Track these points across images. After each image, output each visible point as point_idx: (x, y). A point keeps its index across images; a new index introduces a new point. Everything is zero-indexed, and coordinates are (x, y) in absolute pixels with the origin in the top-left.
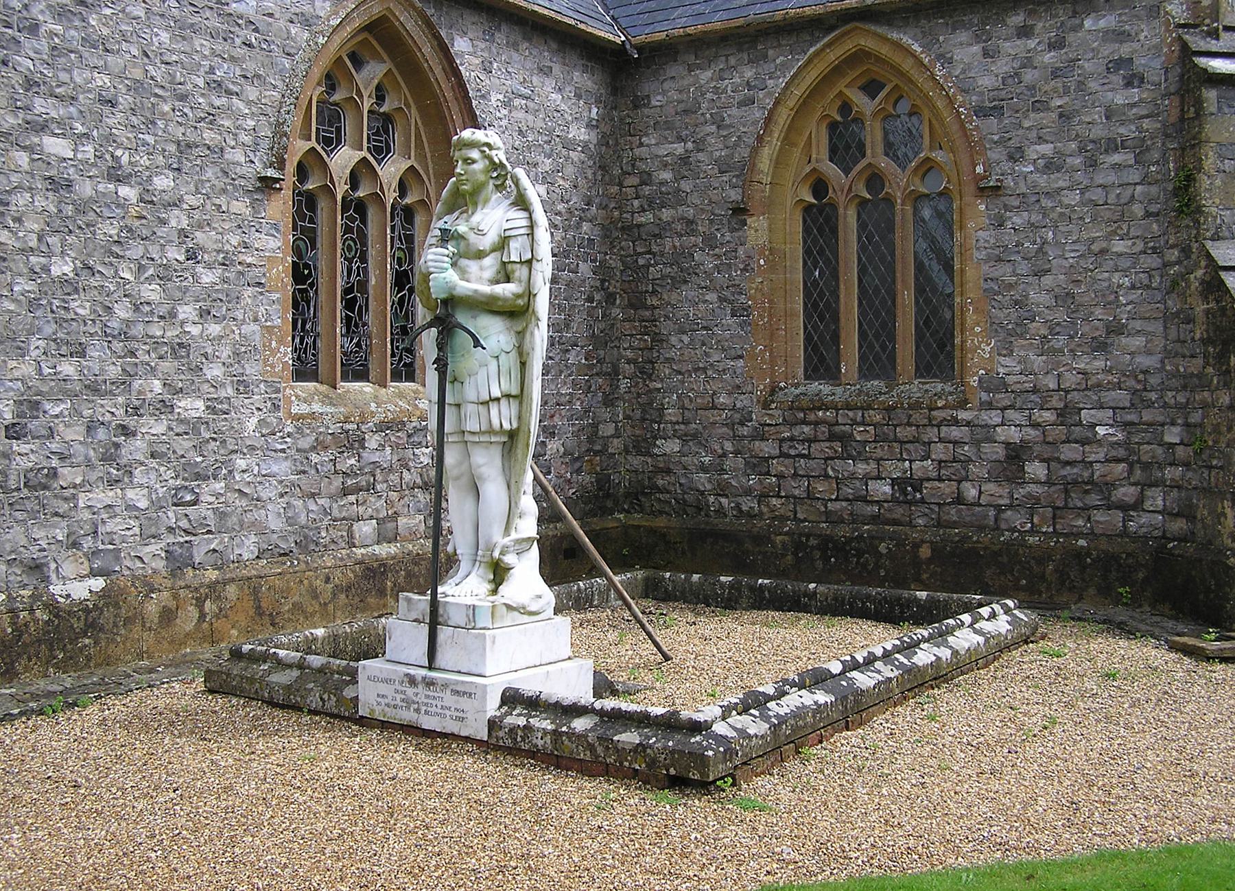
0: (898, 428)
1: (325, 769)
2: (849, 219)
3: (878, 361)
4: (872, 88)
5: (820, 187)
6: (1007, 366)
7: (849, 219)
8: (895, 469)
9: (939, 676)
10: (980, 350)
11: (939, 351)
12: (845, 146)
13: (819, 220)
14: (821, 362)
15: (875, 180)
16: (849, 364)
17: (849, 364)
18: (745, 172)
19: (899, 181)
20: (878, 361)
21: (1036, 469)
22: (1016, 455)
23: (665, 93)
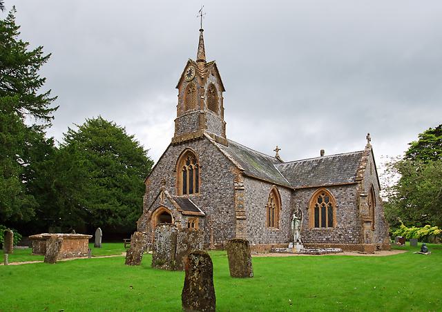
0: (326, 232)
1: (165, 275)
2: (188, 172)
3: (324, 225)
4: (323, 195)
5: (317, 205)
6: (339, 226)
7: (188, 172)
8: (326, 237)
9: (64, 262)
10: (336, 224)
11: (331, 225)
12: (320, 201)
13: (317, 209)
14: (317, 225)
15: (323, 205)
16: (320, 226)
17: (320, 226)
18: (308, 204)
19: (326, 205)
20: (324, 225)
21: (342, 237)
22: (340, 235)
23: (298, 194)
